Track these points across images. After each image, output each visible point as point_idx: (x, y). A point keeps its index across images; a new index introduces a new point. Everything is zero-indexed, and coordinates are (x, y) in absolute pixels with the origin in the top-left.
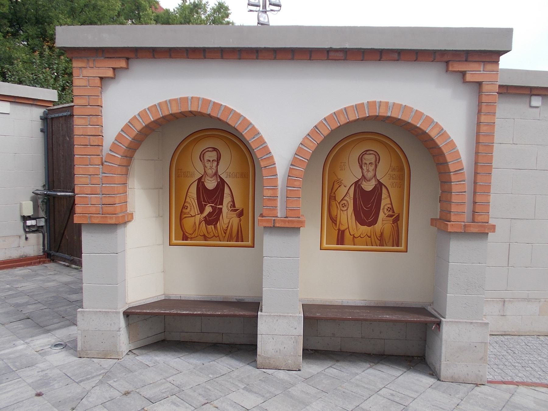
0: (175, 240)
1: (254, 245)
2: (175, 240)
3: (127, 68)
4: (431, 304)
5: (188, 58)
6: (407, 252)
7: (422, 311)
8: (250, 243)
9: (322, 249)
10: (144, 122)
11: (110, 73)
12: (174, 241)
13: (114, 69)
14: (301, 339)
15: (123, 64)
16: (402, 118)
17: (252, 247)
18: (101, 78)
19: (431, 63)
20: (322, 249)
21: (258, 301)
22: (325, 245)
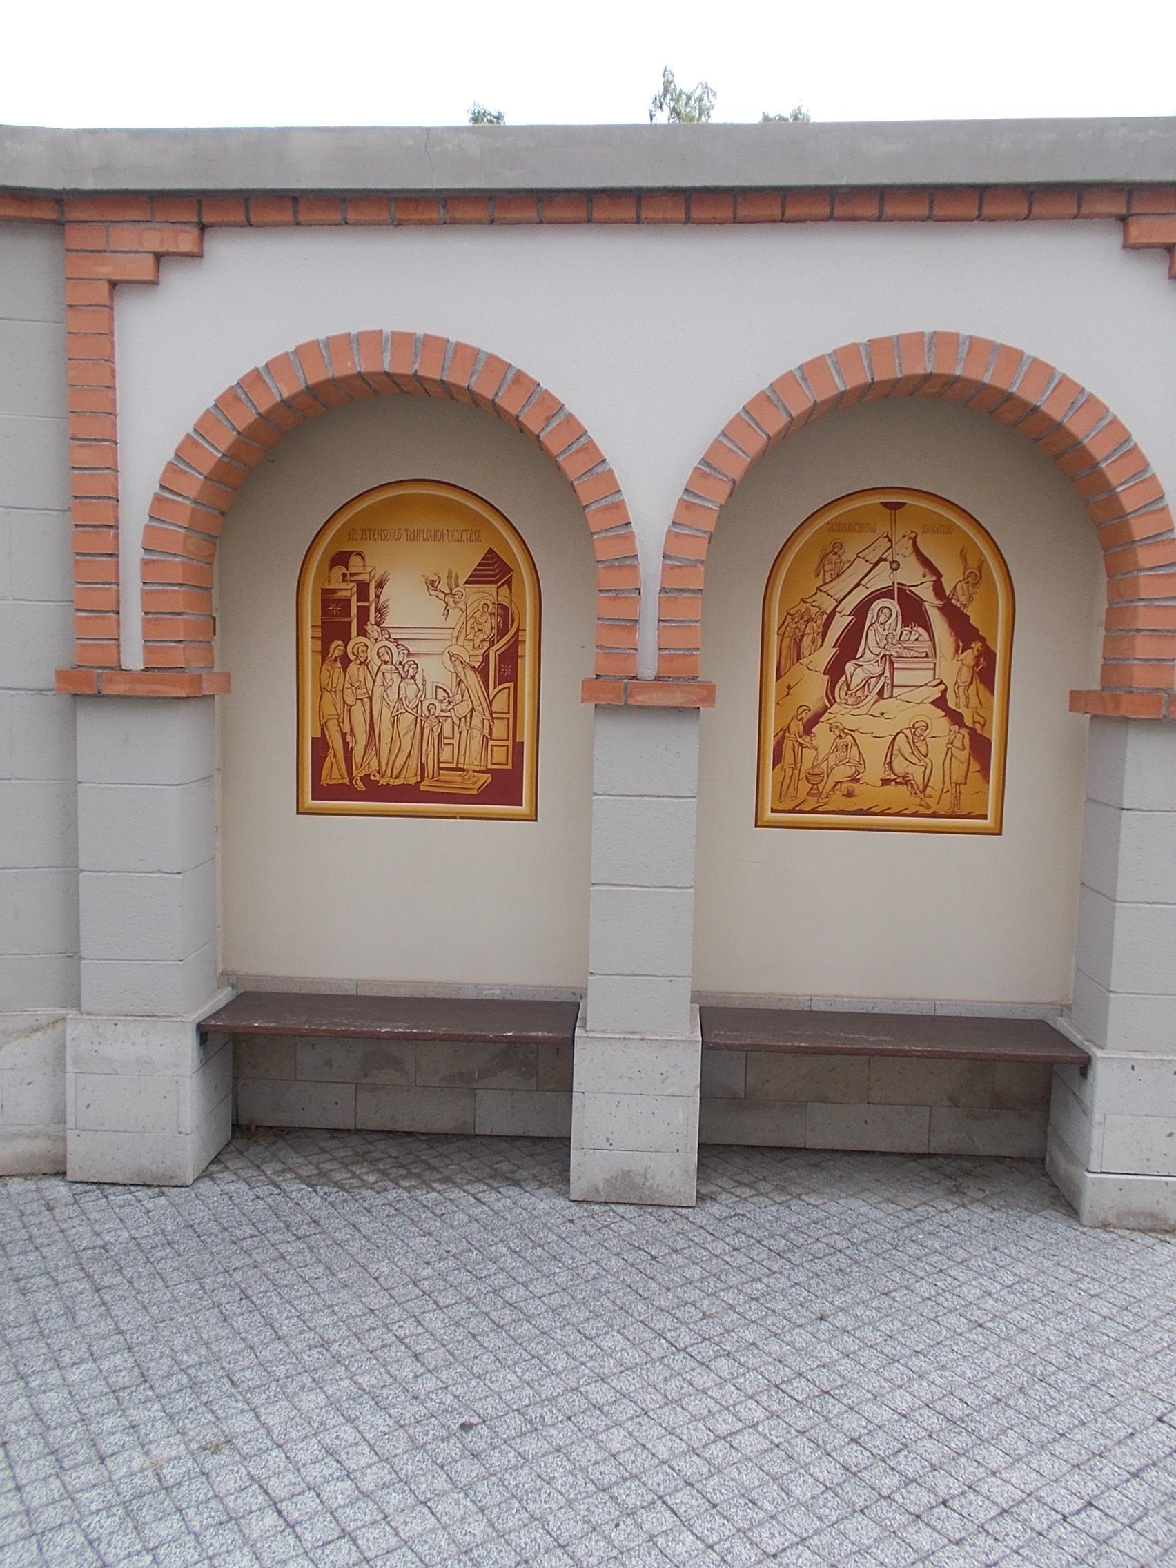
0: (313, 799)
1: (536, 815)
2: (313, 799)
3: (199, 256)
4: (1065, 1009)
5: (298, 224)
6: (1000, 834)
7: (1039, 1030)
8: (988, 823)
9: (300, 810)
10: (871, 369)
11: (142, 267)
12: (310, 802)
13: (158, 257)
14: (694, 1127)
15: (186, 242)
16: (1020, 394)
17: (298, 809)
18: (113, 284)
19: (1071, 222)
20: (300, 810)
21: (573, 999)
22: (524, 809)
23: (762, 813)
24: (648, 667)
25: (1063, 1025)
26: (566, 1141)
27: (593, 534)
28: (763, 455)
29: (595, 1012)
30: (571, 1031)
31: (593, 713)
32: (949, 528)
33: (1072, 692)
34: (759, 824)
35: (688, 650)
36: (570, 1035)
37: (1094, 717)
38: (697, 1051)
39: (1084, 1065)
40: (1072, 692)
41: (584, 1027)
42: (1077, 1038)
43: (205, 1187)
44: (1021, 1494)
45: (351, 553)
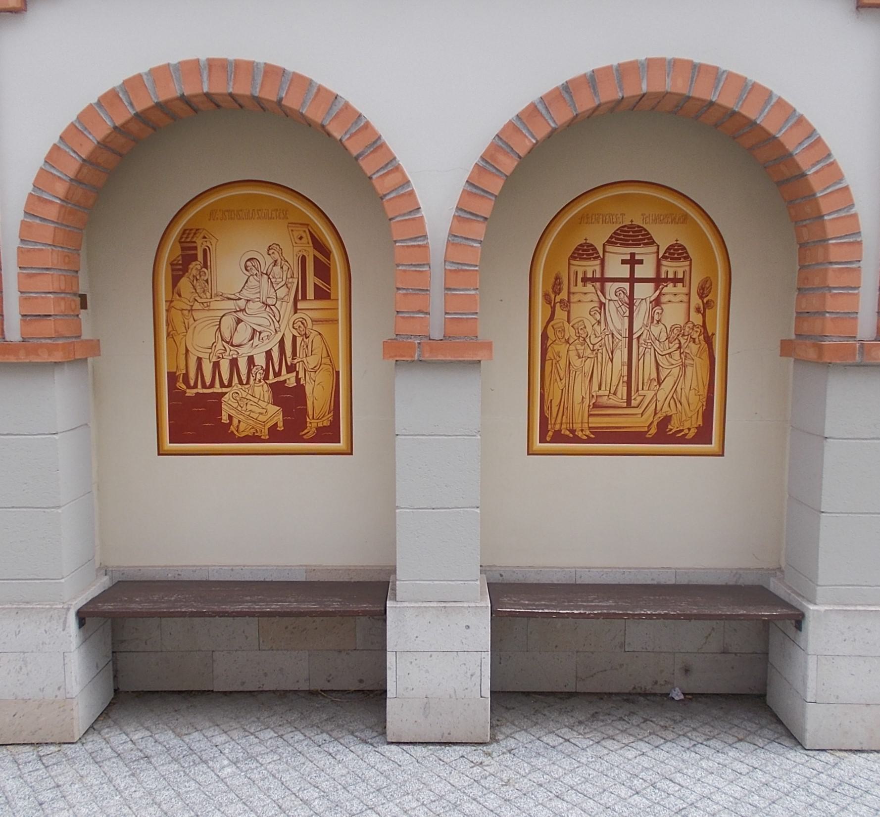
22: (342, 445)
23: (533, 443)
24: (437, 333)
25: (775, 586)
26: (382, 693)
27: (395, 242)
28: (568, 126)
29: (403, 584)
30: (383, 605)
31: (394, 365)
32: (685, 218)
33: (782, 340)
34: (530, 453)
35: (387, 165)
36: (383, 609)
37: (795, 359)
38: (488, 655)
39: (798, 620)
40: (782, 340)
41: (395, 599)
42: (795, 600)
43: (94, 743)
44: (663, 748)
45: (687, 258)
